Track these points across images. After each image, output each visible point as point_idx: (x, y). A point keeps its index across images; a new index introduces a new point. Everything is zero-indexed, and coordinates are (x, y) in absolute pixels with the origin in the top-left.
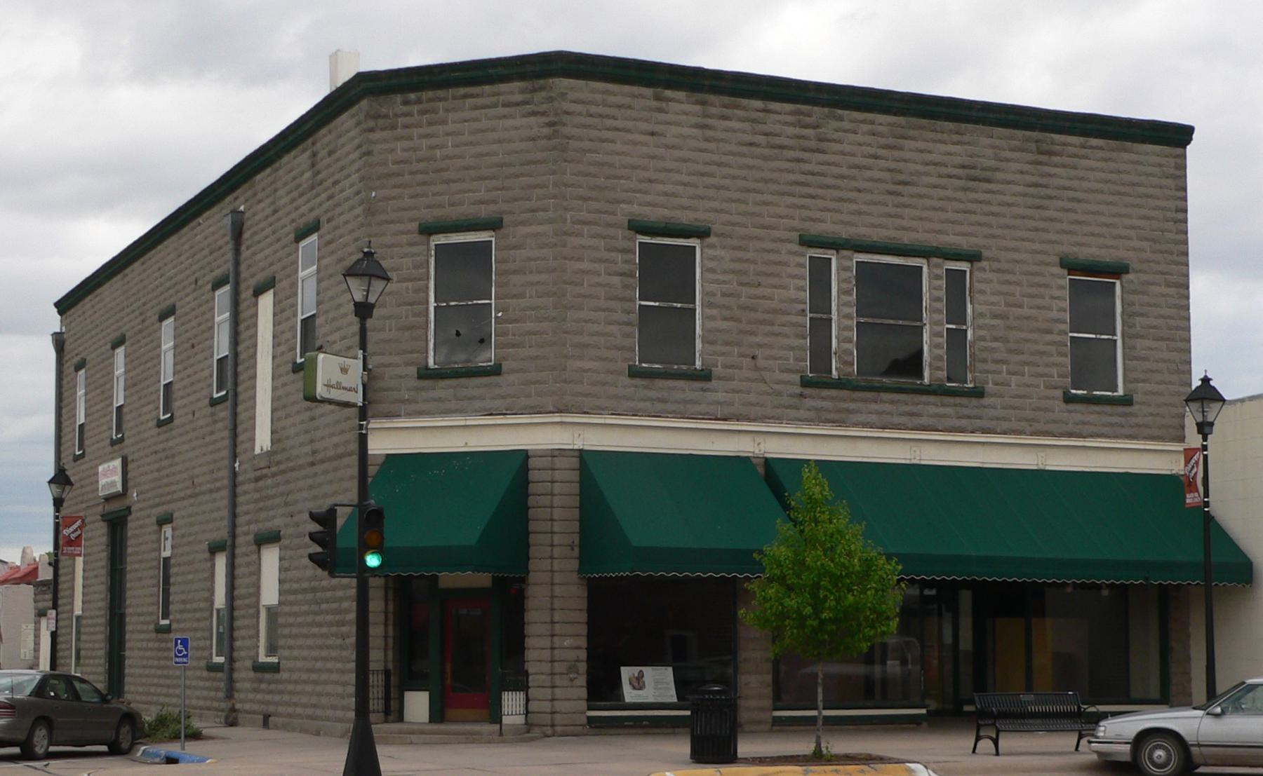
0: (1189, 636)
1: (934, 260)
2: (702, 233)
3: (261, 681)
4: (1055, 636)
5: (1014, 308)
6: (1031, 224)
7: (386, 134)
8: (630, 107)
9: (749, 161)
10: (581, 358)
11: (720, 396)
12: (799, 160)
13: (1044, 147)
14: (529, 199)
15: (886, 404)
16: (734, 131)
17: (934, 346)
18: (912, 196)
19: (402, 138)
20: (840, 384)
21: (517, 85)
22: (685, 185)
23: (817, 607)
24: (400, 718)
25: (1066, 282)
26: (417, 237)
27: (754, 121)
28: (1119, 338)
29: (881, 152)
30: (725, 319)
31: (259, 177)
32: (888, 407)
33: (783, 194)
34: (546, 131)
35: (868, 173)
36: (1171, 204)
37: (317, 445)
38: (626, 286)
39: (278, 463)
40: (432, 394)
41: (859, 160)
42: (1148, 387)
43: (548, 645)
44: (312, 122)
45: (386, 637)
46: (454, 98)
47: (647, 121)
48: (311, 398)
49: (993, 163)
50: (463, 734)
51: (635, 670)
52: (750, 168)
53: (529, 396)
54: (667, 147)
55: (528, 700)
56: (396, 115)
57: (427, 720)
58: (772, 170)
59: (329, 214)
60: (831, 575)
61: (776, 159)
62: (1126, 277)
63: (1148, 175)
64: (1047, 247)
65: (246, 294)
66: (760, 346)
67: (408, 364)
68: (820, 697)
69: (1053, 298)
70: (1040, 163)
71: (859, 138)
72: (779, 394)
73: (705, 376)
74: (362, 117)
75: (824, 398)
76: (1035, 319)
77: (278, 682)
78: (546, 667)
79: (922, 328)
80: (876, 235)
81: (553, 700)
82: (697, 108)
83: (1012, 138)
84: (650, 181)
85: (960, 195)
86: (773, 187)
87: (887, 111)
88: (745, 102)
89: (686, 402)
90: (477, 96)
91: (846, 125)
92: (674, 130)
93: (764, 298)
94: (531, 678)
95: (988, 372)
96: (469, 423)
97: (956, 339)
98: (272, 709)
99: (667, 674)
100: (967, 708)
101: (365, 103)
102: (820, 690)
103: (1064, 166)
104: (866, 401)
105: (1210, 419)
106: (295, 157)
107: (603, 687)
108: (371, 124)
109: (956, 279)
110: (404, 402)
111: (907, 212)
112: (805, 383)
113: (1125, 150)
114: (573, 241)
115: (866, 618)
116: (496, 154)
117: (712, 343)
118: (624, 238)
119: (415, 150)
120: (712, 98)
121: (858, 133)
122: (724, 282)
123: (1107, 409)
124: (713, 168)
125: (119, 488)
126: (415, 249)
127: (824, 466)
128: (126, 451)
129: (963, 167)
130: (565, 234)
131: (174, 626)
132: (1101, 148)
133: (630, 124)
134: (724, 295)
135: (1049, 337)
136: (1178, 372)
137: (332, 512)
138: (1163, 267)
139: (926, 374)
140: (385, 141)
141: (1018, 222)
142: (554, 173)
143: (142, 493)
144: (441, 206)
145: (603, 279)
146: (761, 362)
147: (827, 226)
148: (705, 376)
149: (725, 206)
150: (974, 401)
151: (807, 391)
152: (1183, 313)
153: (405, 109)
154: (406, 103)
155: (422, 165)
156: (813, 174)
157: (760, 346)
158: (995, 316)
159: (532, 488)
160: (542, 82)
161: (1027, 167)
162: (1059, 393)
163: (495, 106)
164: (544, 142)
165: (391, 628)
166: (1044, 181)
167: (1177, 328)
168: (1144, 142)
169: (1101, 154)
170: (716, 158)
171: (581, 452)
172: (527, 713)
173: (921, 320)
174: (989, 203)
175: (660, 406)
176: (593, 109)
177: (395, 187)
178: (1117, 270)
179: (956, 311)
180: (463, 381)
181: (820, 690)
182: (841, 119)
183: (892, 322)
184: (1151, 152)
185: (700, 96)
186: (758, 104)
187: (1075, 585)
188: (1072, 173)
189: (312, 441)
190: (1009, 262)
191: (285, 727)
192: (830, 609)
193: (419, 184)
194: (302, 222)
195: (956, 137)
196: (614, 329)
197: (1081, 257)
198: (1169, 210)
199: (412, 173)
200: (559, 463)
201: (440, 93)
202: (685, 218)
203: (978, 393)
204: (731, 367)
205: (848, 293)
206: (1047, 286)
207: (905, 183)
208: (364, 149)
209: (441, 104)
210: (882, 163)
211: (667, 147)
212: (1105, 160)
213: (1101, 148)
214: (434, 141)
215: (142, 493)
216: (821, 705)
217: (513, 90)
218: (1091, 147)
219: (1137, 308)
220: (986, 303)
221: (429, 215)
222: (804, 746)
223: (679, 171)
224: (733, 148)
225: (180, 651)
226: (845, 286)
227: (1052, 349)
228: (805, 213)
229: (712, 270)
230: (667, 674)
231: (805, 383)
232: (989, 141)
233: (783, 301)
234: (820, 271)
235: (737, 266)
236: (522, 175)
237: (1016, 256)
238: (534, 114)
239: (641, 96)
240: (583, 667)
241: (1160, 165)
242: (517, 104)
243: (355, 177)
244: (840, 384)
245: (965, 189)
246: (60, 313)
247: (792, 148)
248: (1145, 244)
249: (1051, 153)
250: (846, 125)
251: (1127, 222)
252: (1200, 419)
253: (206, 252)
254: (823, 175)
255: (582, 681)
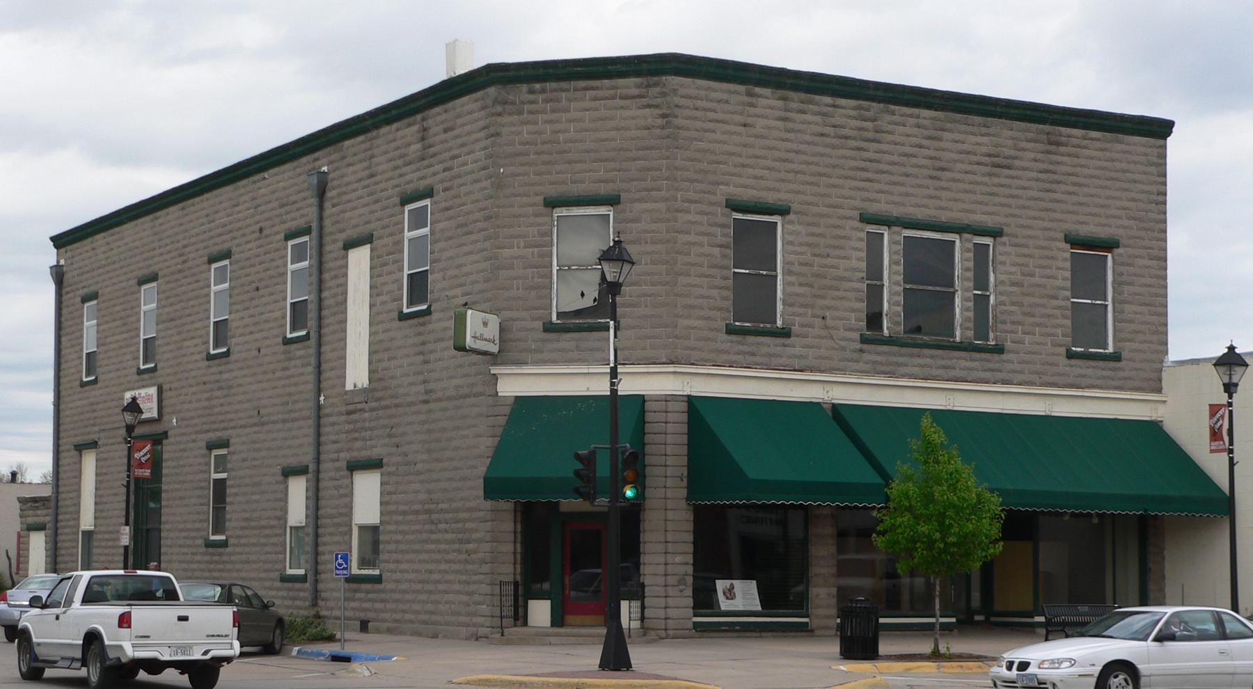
0: (1163, 558)
1: (966, 236)
2: (783, 211)
3: (356, 591)
4: (1052, 556)
5: (1023, 278)
6: (1042, 204)
7: (515, 118)
8: (727, 102)
9: (820, 149)
10: (689, 317)
11: (797, 350)
12: (859, 149)
13: (1053, 138)
14: (644, 180)
15: (928, 358)
16: (809, 123)
17: (964, 309)
18: (949, 181)
19: (528, 123)
20: (890, 341)
21: (632, 81)
22: (769, 169)
23: (944, 530)
24: (525, 624)
25: (1068, 255)
26: (542, 209)
27: (825, 115)
28: (1110, 303)
29: (925, 142)
30: (801, 285)
31: (347, 143)
32: (928, 361)
33: (847, 178)
34: (660, 121)
35: (914, 160)
36: (1154, 188)
37: (431, 386)
38: (724, 256)
39: (379, 399)
40: (555, 345)
41: (908, 150)
42: (1135, 346)
43: (662, 560)
44: (423, 101)
45: (515, 553)
46: (576, 90)
47: (741, 114)
48: (461, 348)
49: (1012, 153)
50: (581, 636)
51: (727, 583)
52: (822, 155)
53: (645, 349)
54: (756, 136)
55: (643, 608)
56: (522, 103)
57: (549, 624)
58: (839, 157)
59: (446, 184)
60: (954, 506)
61: (842, 147)
62: (1116, 251)
63: (1136, 163)
64: (1055, 225)
65: (332, 248)
66: (829, 308)
67: (533, 319)
68: (937, 607)
69: (1058, 268)
70: (1049, 152)
71: (907, 130)
72: (843, 349)
73: (785, 333)
74: (489, 102)
75: (878, 353)
76: (1044, 286)
77: (383, 591)
78: (661, 580)
79: (954, 293)
80: (920, 214)
81: (666, 608)
82: (780, 103)
83: (1028, 131)
84: (743, 166)
85: (986, 179)
86: (839, 172)
87: (929, 106)
88: (817, 98)
89: (770, 355)
90: (597, 88)
91: (896, 118)
92: (761, 122)
93: (832, 267)
94: (646, 589)
95: (1007, 332)
96: (591, 371)
97: (981, 302)
98: (370, 615)
99: (752, 585)
100: (977, 618)
101: (492, 91)
102: (937, 601)
103: (1069, 155)
104: (911, 356)
105: (1235, 380)
106: (398, 130)
107: (704, 600)
108: (499, 109)
109: (981, 250)
110: (530, 351)
111: (944, 194)
112: (864, 340)
113: (1122, 142)
114: (683, 217)
115: (981, 543)
116: (614, 140)
117: (791, 305)
118: (723, 215)
119: (539, 133)
120: (792, 94)
121: (907, 124)
122: (801, 253)
123: (1101, 364)
124: (792, 155)
125: (155, 414)
126: (539, 220)
127: (940, 416)
128: (161, 380)
129: (990, 155)
130: (678, 211)
131: (231, 541)
132: (1099, 140)
133: (728, 117)
134: (801, 264)
135: (1055, 303)
136: (1157, 332)
137: (593, 453)
138: (1147, 243)
139: (958, 333)
140: (513, 124)
141: (1031, 203)
142: (667, 158)
143: (183, 419)
144: (564, 183)
145: (707, 250)
146: (829, 322)
147: (881, 207)
148: (785, 333)
149: (801, 188)
150: (996, 357)
151: (865, 347)
152: (1162, 283)
153: (531, 97)
154: (531, 92)
155: (546, 147)
156: (871, 161)
157: (829, 308)
158: (1013, 284)
159: (648, 428)
160: (656, 79)
161: (1039, 156)
162: (1063, 350)
163: (613, 98)
164: (658, 131)
165: (519, 546)
166: (1051, 167)
167: (1157, 295)
168: (1133, 134)
169: (1098, 144)
170: (794, 146)
171: (689, 396)
172: (643, 619)
173: (952, 286)
174: (1010, 187)
175: (750, 359)
176: (699, 103)
177: (523, 165)
178: (1109, 245)
179: (981, 281)
180: (585, 334)
181: (937, 601)
182: (893, 113)
183: (930, 288)
184: (1138, 143)
185: (781, 92)
186: (828, 100)
187: (1073, 515)
188: (1076, 160)
189: (425, 382)
190: (1024, 237)
191: (378, 631)
192: (954, 534)
193: (544, 163)
194: (410, 187)
195: (984, 130)
196: (715, 292)
197: (1082, 233)
198: (1151, 193)
199: (536, 153)
200: (672, 406)
201: (564, 85)
202: (770, 198)
203: (999, 350)
204: (806, 326)
205: (897, 263)
206: (1053, 258)
207: (943, 169)
208: (492, 130)
209: (564, 95)
210: (926, 152)
211: (756, 136)
212: (1101, 150)
213: (1099, 140)
214: (557, 126)
215: (183, 419)
216: (938, 613)
217: (630, 84)
218: (1092, 139)
219: (1125, 278)
220: (1006, 273)
221: (553, 191)
222: (926, 647)
223: (765, 158)
224: (808, 138)
225: (340, 565)
226: (895, 257)
227: (1057, 312)
228: (865, 194)
229: (791, 243)
230: (752, 585)
231: (864, 340)
232: (1010, 133)
233: (846, 270)
234: (874, 243)
235: (811, 239)
236: (638, 159)
237: (1030, 232)
238: (649, 106)
239: (735, 92)
240: (690, 580)
241: (1146, 155)
242: (633, 97)
243: (480, 154)
244: (890, 341)
245: (990, 175)
246: (56, 246)
247: (854, 139)
248: (1132, 222)
249: (1058, 144)
250: (896, 118)
251: (1119, 203)
252: (1226, 380)
253: (275, 204)
254: (878, 162)
255: (689, 592)
